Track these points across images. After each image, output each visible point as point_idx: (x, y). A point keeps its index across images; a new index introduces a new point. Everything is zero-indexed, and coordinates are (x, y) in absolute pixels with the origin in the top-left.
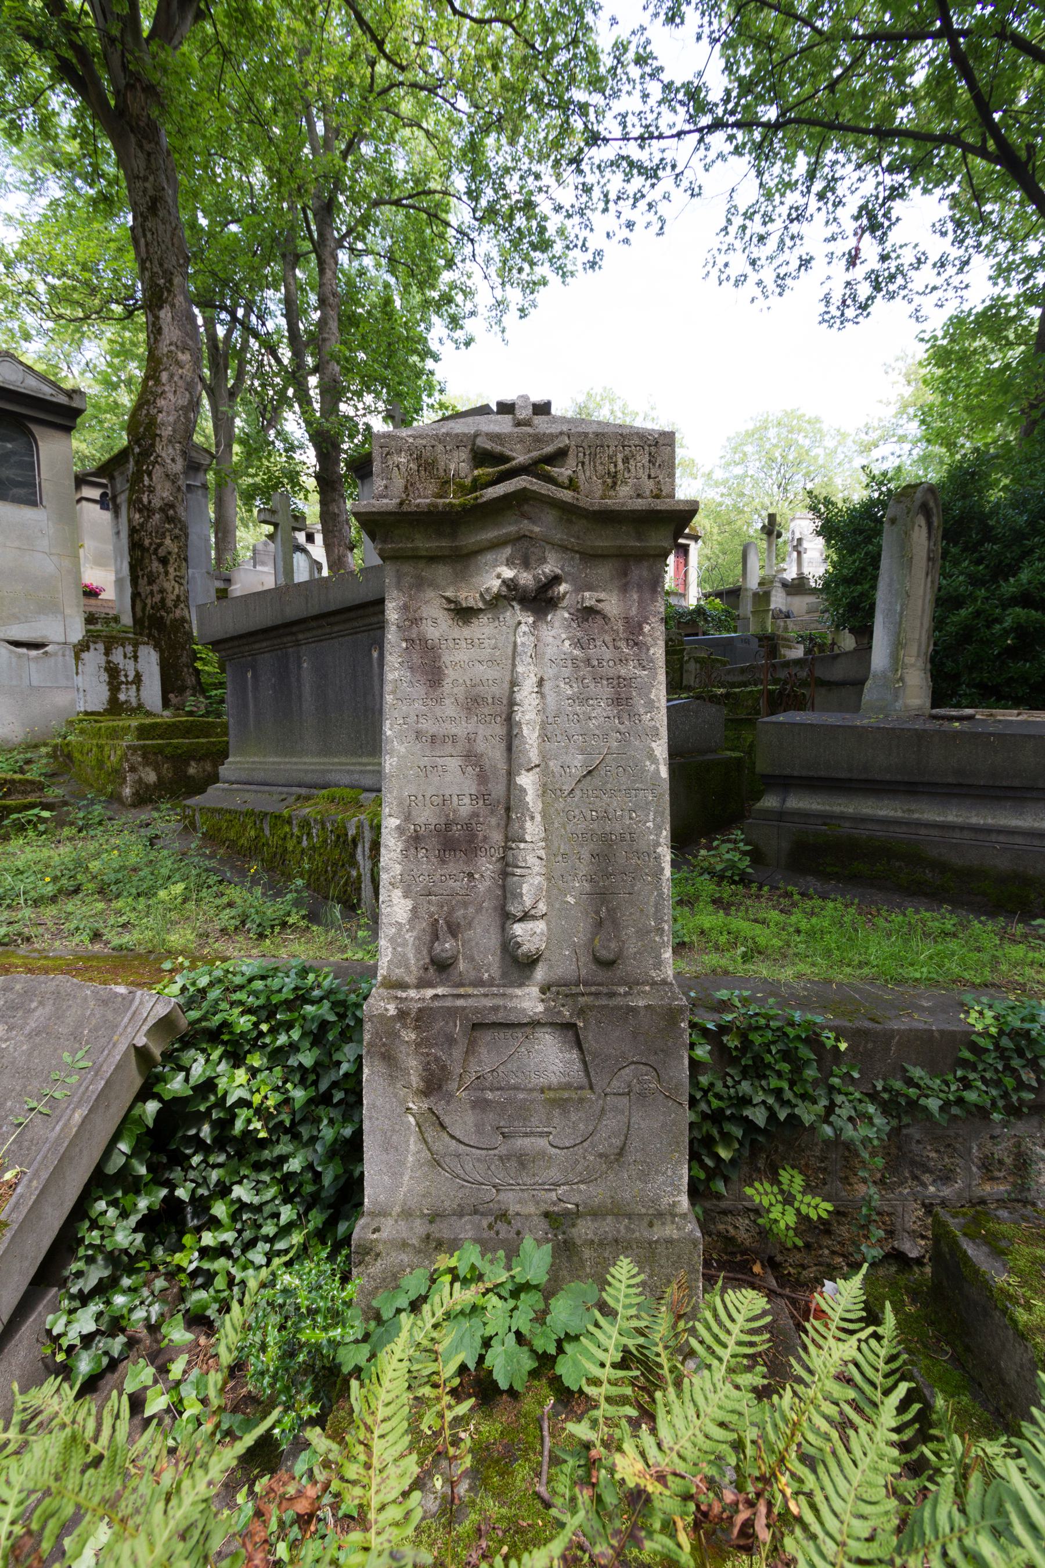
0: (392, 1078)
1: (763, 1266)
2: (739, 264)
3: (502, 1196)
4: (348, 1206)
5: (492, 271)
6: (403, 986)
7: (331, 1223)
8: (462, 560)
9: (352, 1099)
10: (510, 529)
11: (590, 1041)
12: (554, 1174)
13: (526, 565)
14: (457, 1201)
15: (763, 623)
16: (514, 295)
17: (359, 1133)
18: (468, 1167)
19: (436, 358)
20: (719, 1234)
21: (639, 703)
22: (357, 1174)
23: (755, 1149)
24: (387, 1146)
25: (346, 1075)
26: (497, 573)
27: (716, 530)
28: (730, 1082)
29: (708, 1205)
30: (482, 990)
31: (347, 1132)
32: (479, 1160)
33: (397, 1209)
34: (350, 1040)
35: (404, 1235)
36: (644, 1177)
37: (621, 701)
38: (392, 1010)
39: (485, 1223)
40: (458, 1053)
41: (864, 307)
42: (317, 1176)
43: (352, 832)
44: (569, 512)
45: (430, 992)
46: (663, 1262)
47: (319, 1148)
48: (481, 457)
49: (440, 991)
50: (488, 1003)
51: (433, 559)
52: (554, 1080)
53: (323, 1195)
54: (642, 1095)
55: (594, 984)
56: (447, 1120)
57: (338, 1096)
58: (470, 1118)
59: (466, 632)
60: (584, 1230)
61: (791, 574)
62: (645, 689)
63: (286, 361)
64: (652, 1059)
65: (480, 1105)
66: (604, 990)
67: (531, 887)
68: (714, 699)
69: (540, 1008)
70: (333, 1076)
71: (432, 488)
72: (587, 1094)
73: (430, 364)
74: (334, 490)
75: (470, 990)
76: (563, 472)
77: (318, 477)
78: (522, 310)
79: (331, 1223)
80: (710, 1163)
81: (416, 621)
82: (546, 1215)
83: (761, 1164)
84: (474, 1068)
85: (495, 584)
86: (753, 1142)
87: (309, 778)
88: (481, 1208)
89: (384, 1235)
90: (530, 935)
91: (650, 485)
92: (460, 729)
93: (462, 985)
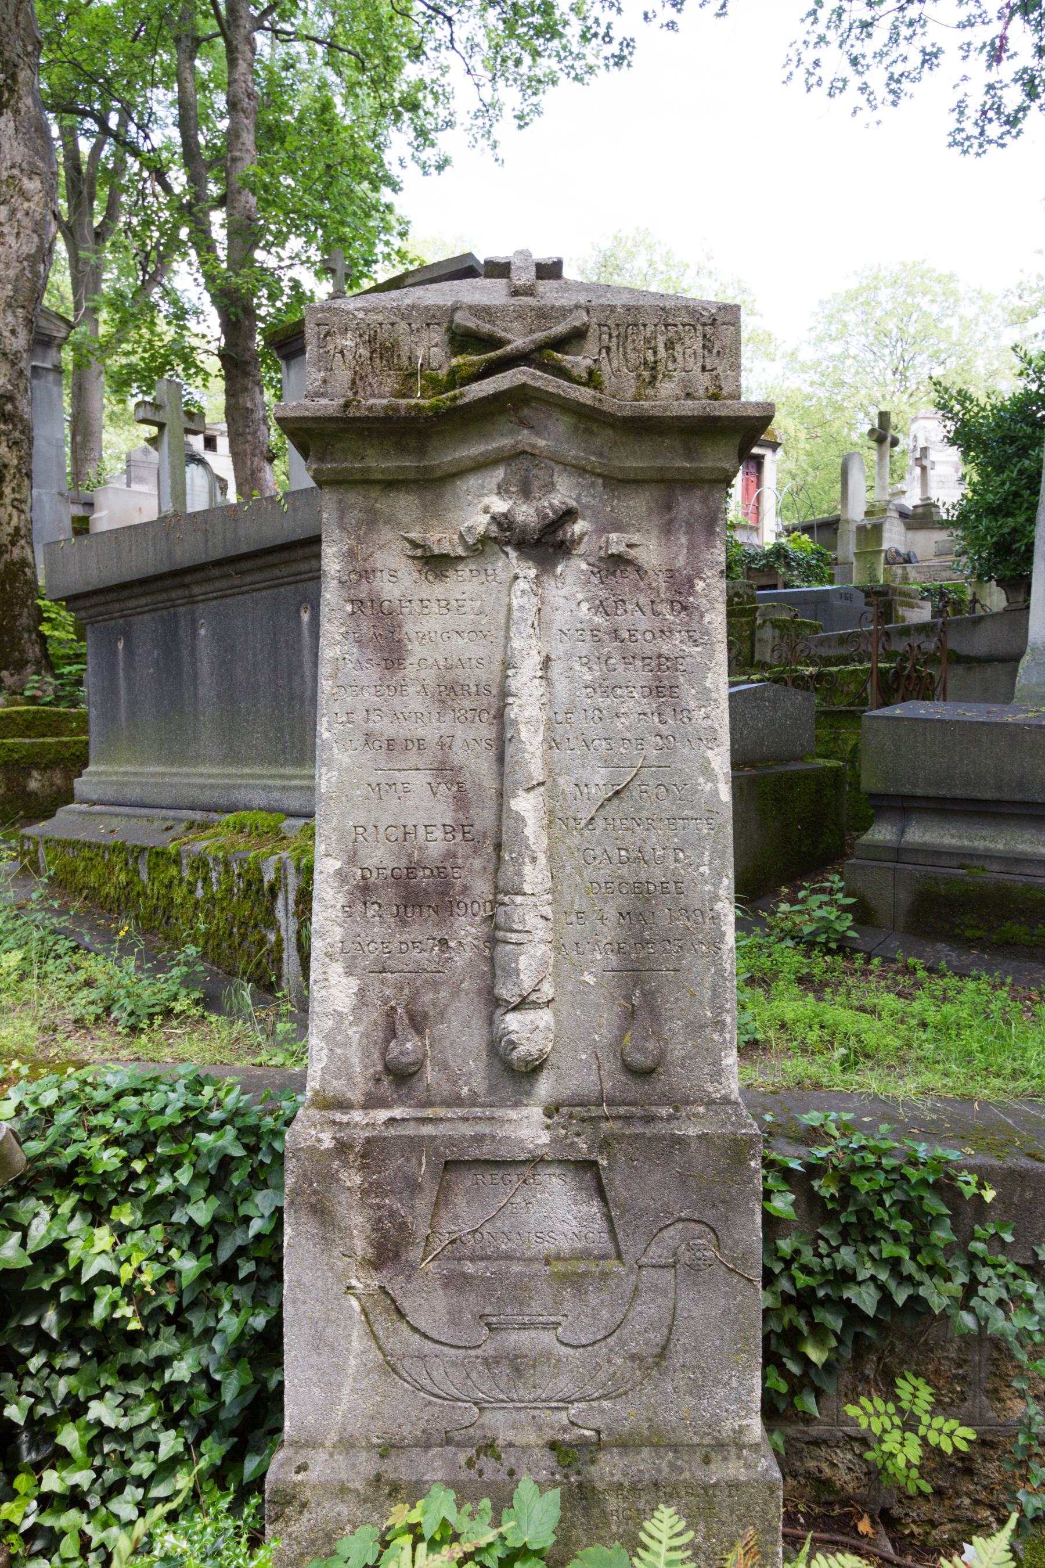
1: (873, 1523)
2: (834, 62)
3: (488, 1418)
5: (476, 62)
6: (343, 1105)
7: (234, 1457)
8: (433, 485)
9: (267, 1273)
10: (503, 442)
11: (618, 1186)
12: (564, 1385)
13: (526, 492)
14: (422, 1425)
15: (872, 570)
16: (510, 97)
18: (438, 1375)
19: (395, 186)
20: (808, 1475)
21: (689, 695)
22: (272, 1384)
24: (318, 1343)
25: (259, 1237)
26: (483, 504)
27: (803, 435)
30: (460, 1112)
31: (259, 1322)
32: (453, 1364)
33: (333, 1437)
34: (265, 1185)
35: (343, 1475)
36: (697, 1389)
37: (662, 690)
39: (462, 1458)
40: (423, 1204)
41: (1012, 121)
42: (215, 1388)
43: (269, 876)
44: (588, 419)
45: (382, 1115)
46: (724, 1516)
47: (217, 1344)
48: (462, 340)
49: (398, 1113)
50: (468, 1130)
51: (391, 484)
52: (565, 1245)
53: (223, 1415)
56: (406, 1305)
57: (246, 1268)
58: (441, 1301)
59: (439, 589)
60: (608, 1468)
61: (912, 500)
62: (696, 676)
63: (177, 189)
64: (709, 1215)
65: (456, 1282)
67: (530, 962)
68: (800, 683)
69: (545, 1138)
71: (391, 383)
73: (386, 195)
74: (247, 374)
75: (442, 1112)
76: (578, 362)
77: (222, 355)
78: (520, 117)
79: (234, 1457)
80: (794, 1368)
81: (366, 574)
82: (553, 1446)
83: (870, 1370)
84: (447, 1227)
85: (481, 522)
86: (858, 1337)
87: (207, 797)
88: (456, 1436)
90: (528, 1030)
91: (704, 381)
92: (431, 730)
93: (429, 1104)
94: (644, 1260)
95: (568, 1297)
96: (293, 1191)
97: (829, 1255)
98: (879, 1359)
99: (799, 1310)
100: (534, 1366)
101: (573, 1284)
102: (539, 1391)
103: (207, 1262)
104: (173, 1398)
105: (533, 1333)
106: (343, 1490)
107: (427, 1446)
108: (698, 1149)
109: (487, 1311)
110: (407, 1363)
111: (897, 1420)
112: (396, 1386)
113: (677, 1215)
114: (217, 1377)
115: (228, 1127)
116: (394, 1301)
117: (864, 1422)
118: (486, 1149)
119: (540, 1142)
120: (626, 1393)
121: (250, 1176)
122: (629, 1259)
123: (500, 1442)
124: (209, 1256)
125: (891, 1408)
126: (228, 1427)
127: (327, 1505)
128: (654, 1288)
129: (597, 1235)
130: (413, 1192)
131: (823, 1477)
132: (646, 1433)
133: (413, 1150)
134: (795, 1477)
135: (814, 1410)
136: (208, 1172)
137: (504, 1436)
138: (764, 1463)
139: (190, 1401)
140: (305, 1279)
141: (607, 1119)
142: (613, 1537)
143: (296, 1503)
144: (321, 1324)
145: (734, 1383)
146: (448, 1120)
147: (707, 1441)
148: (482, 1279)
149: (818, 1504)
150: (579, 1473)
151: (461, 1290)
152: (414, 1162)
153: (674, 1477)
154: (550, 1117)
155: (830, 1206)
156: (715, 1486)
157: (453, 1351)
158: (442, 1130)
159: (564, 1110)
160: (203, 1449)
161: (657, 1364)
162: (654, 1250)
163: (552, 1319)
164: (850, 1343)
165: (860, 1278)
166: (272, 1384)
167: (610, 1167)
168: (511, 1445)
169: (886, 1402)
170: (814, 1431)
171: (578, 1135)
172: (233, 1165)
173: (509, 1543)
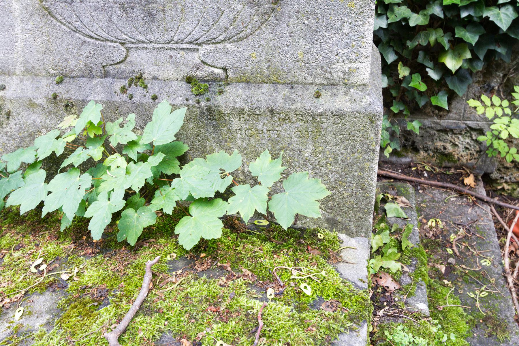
1: (476, 179)
14: (83, 60)
18: (86, 19)
20: (436, 150)
23: (492, 63)
29: (428, 122)
35: (30, 94)
36: (312, 35)
39: (118, 85)
46: (330, 138)
60: (232, 98)
80: (434, 75)
82: (189, 80)
83: (495, 83)
86: (491, 54)
98: (505, 76)
99: (445, 32)
100: (163, 11)
102: (172, 34)
106: (32, 105)
107: (91, 76)
111: (508, 111)
112: (54, 27)
125: (505, 103)
131: (446, 152)
132: (266, 72)
134: (426, 151)
137: (149, 71)
138: (368, 99)
145: (346, 29)
149: (440, 167)
150: (208, 100)
153: (287, 106)
156: (321, 115)
168: (155, 78)
169: (502, 99)
170: (444, 123)
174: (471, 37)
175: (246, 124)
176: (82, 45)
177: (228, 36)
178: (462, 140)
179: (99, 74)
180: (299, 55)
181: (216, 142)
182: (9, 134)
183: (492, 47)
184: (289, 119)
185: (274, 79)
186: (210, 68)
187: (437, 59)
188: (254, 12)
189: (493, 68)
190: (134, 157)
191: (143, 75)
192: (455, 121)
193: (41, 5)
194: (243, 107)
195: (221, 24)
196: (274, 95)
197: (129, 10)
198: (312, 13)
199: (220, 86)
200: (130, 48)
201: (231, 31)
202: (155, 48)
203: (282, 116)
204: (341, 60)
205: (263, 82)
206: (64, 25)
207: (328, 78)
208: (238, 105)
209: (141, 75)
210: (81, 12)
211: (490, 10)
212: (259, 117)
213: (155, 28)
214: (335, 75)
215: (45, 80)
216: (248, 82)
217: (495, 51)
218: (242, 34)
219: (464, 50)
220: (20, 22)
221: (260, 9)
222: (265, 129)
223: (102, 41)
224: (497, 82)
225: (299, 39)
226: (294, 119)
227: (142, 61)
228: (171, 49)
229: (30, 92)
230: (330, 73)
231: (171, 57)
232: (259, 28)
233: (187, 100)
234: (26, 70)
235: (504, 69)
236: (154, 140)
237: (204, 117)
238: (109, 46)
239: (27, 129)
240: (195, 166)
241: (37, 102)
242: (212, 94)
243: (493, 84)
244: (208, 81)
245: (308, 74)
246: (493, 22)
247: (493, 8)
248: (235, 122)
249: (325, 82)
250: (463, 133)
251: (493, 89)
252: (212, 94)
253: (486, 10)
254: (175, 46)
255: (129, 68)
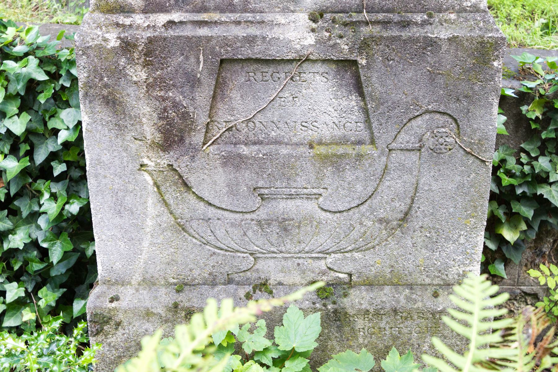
0: (120, 128)
3: (260, 265)
4: (84, 287)
7: (65, 303)
9: (76, 174)
11: (374, 82)
12: (324, 240)
14: (208, 269)
17: (86, 211)
18: (220, 233)
22: (89, 253)
24: (119, 209)
25: (66, 145)
28: (524, 158)
30: (234, 16)
31: (74, 208)
32: (232, 225)
33: (137, 278)
34: (67, 105)
35: (148, 304)
36: (432, 245)
38: (113, 43)
40: (203, 96)
42: (44, 254)
45: (162, 18)
47: (42, 221)
49: (176, 16)
50: (240, 32)
52: (326, 133)
53: (53, 273)
54: (435, 151)
55: (382, 10)
56: (192, 180)
57: (59, 169)
58: (221, 176)
60: (357, 300)
64: (453, 108)
65: (233, 161)
66: (396, 18)
69: (311, 39)
70: (51, 146)
72: (367, 149)
75: (216, 16)
79: (65, 303)
84: (223, 117)
88: (236, 277)
89: (123, 304)
93: (204, 9)
94: (394, 145)
95: (328, 174)
96: (86, 84)
97: (527, 164)
99: (499, 205)
100: (299, 227)
101: (332, 164)
102: (303, 245)
103: (25, 162)
104: (13, 261)
105: (298, 202)
108: (448, 51)
109: (260, 185)
110: (195, 224)
113: (424, 108)
114: (45, 245)
115: (31, 57)
116: (181, 177)
117: (542, 281)
118: (257, 49)
119: (306, 43)
120: (374, 247)
121: (54, 95)
122: (381, 143)
123: (272, 282)
124: (28, 158)
126: (58, 282)
127: (137, 324)
128: (402, 167)
129: (354, 125)
130: (193, 87)
132: (389, 276)
133: (191, 48)
135: (503, 274)
136: (18, 94)
139: (26, 263)
140: (104, 158)
141: (367, 23)
142: (360, 347)
143: (112, 323)
144: (120, 194)
145: (462, 240)
146: (221, 23)
147: (436, 282)
148: (255, 159)
150: (334, 303)
151: (237, 168)
152: (192, 60)
153: (410, 306)
154: (315, 21)
155: (533, 126)
157: (232, 215)
158: (215, 32)
159: (328, 16)
160: (40, 295)
161: (400, 226)
162: (403, 137)
163: (315, 191)
164: (536, 229)
165: (551, 180)
166: (89, 253)
167: (368, 66)
168: (280, 284)
171: (341, 37)
172: (39, 89)
173: (281, 348)
174: (527, 211)
175: (369, 323)
176: (211, 255)
177: (357, 246)
178: (517, 305)
179: (223, 281)
180: (420, 261)
181: (337, 341)
182: (112, 345)
183: (544, 218)
184: (411, 317)
185: (397, 282)
186: (336, 273)
187: (494, 232)
188: (383, 227)
189: (543, 234)
190: (269, 363)
191: (269, 282)
192: (509, 287)
193: (176, 222)
194: (368, 308)
195: (352, 237)
196: (396, 296)
197: (266, 226)
198: (434, 228)
199: (344, 289)
200: (259, 257)
201: (361, 242)
202: (283, 258)
203: (404, 314)
204: (457, 265)
205: (385, 284)
206: (196, 238)
207: (444, 280)
208: (363, 307)
209: (267, 280)
210: (217, 228)
211: (543, 187)
212: (383, 316)
213: (288, 241)
214: (450, 277)
215: (164, 289)
216: (371, 285)
217: (547, 221)
218: (370, 245)
219: (519, 222)
220: (150, 236)
221: (388, 225)
222: (387, 327)
223: (231, 252)
224: (548, 247)
225: (421, 248)
226: (416, 317)
227: (270, 269)
228: (299, 258)
229: (147, 302)
230: (447, 275)
231: (299, 264)
232: (386, 240)
233: (314, 303)
234: (144, 280)
235: (554, 235)
236: (294, 346)
237: (329, 319)
238: (239, 257)
239: (135, 338)
240: (331, 368)
241: (155, 312)
242: (337, 297)
243: (544, 250)
244: (333, 285)
245: (427, 276)
246: (547, 199)
247: (544, 186)
248: (359, 322)
249: (442, 283)
250: (518, 298)
251: (544, 253)
252: (337, 297)
253: (540, 187)
254: (304, 255)
255: (255, 275)
